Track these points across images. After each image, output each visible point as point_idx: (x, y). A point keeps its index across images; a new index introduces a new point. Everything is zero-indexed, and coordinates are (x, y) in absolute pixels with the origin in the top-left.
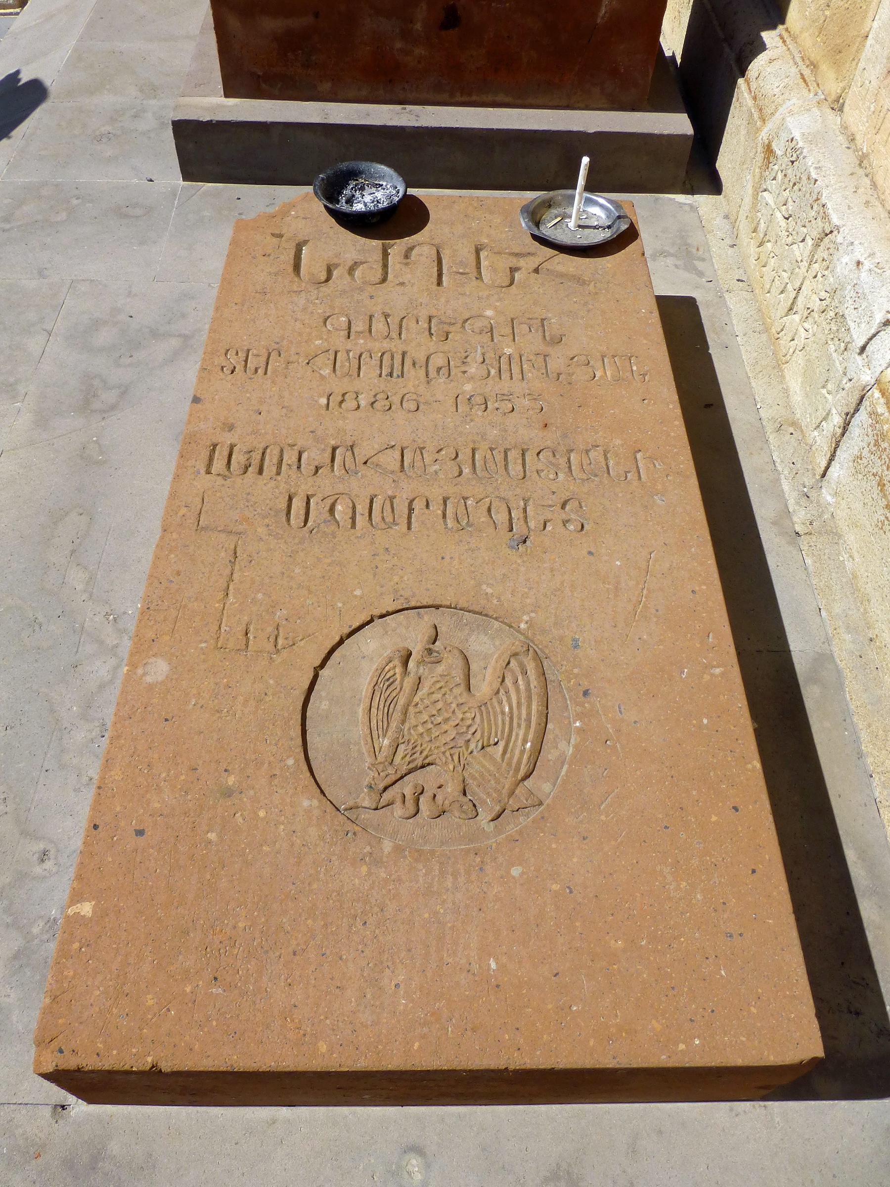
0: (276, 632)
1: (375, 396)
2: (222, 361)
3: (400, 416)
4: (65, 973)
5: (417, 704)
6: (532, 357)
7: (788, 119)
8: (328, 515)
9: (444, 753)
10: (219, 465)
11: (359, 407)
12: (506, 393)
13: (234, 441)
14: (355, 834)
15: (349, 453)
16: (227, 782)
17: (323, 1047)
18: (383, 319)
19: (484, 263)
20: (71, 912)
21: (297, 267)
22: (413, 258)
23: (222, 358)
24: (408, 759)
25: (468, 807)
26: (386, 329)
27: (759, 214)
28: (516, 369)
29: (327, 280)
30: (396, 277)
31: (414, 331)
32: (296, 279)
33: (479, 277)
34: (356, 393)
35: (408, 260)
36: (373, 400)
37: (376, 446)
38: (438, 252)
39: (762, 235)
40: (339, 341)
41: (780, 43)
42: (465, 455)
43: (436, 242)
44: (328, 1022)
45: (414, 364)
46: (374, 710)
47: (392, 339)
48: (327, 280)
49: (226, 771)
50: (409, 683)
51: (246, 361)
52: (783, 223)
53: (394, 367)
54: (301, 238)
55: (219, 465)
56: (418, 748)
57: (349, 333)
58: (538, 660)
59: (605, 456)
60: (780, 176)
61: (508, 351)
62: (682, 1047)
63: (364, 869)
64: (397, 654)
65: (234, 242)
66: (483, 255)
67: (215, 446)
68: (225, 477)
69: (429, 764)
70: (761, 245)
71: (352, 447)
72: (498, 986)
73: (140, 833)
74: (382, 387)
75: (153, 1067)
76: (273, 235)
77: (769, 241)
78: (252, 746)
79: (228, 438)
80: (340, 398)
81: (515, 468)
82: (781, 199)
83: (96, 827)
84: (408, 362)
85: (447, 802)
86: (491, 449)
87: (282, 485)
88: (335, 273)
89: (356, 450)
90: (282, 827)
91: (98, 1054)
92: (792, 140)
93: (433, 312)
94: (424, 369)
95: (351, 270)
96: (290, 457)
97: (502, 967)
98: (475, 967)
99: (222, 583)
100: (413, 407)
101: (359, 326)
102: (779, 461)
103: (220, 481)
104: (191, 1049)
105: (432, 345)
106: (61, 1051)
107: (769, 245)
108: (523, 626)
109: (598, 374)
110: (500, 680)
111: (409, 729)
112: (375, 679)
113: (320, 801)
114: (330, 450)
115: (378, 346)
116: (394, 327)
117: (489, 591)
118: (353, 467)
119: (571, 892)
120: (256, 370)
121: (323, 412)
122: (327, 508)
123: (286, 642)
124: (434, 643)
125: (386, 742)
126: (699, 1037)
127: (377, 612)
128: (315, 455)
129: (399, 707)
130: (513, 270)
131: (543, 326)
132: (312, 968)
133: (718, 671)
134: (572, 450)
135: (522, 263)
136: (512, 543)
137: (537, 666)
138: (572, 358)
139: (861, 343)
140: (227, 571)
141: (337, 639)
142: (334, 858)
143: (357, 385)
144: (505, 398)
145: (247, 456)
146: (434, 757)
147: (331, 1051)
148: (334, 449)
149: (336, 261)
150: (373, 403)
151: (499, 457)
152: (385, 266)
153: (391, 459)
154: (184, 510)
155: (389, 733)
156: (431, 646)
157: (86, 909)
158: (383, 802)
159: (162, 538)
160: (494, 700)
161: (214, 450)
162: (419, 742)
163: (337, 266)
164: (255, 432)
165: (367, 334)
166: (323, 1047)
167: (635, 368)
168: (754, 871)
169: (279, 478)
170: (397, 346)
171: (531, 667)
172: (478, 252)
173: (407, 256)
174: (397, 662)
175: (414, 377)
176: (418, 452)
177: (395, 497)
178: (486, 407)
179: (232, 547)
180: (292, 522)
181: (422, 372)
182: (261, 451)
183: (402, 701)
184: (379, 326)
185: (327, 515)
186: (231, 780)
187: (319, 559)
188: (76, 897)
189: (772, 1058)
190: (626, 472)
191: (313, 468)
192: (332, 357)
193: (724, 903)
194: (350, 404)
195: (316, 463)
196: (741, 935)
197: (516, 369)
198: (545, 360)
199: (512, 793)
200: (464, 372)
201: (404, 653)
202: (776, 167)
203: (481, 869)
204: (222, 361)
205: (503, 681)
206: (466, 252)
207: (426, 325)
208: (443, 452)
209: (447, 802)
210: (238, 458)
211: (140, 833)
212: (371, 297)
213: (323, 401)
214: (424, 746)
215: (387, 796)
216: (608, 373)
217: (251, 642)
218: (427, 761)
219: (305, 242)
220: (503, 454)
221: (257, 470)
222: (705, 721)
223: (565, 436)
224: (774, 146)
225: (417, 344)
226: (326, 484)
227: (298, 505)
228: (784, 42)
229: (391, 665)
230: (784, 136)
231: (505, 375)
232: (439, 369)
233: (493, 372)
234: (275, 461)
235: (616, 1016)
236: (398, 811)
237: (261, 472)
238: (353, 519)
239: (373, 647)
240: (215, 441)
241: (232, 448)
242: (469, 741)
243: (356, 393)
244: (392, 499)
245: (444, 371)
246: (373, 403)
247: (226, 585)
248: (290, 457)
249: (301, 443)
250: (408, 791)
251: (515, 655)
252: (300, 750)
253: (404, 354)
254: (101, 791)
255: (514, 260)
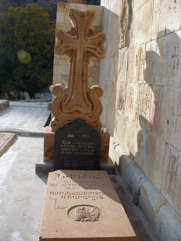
139: (138, 182)
194: (69, 188)
237: (58, 194)
239: (76, 209)
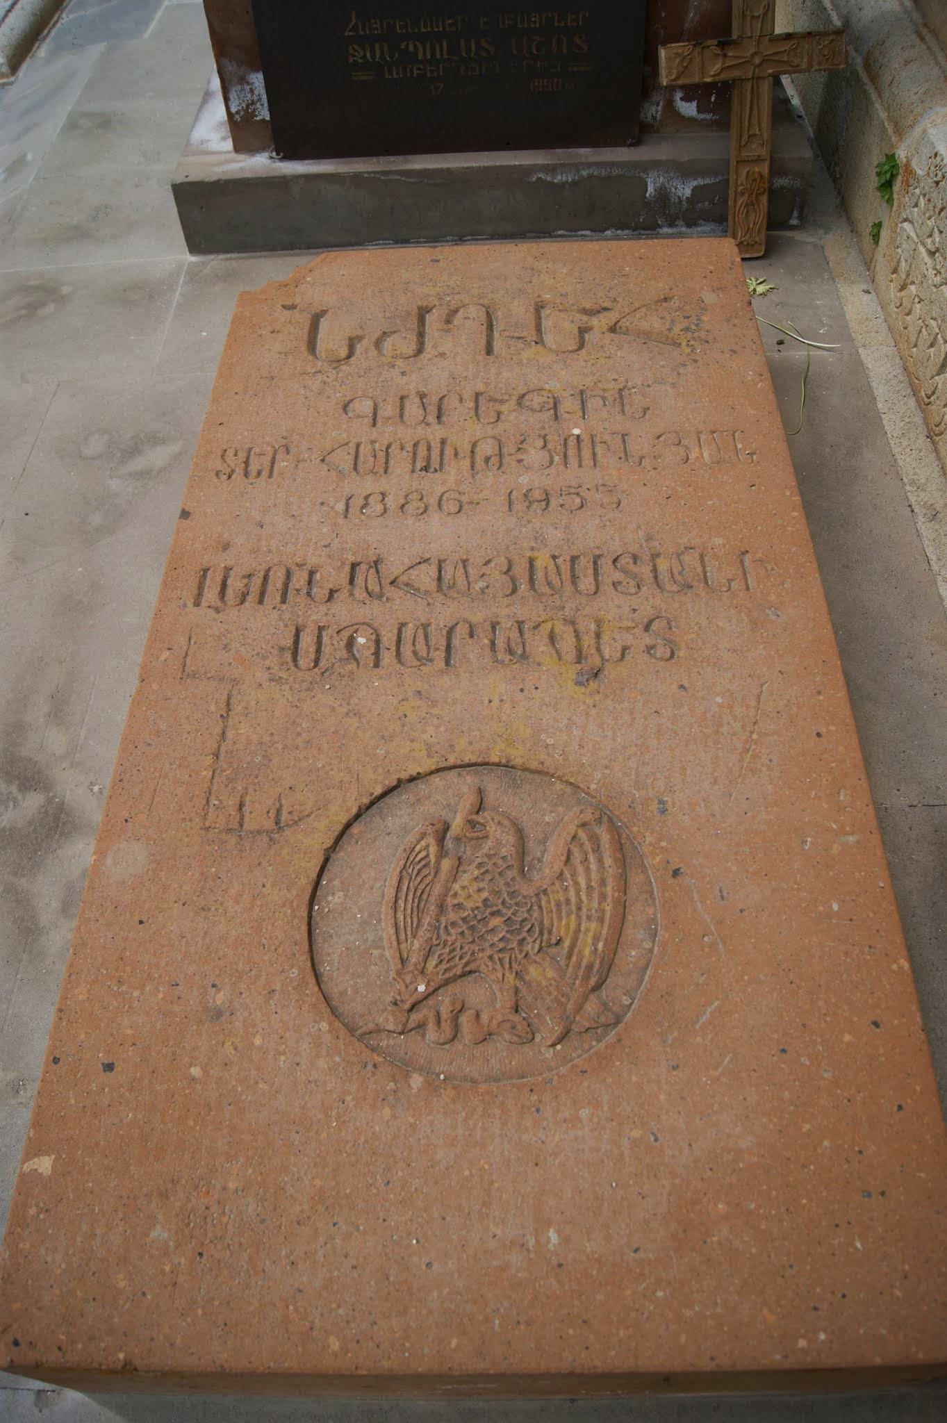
0: (277, 805)
1: (407, 496)
2: (218, 464)
3: (435, 518)
4: (21, 1246)
5: (455, 895)
6: (607, 438)
7: (930, 131)
8: (344, 651)
9: (491, 957)
10: (211, 595)
11: (385, 511)
12: (573, 484)
13: (229, 563)
14: (375, 1066)
15: (373, 571)
16: (214, 1001)
17: (335, 1344)
18: (417, 400)
19: (547, 324)
20: (27, 1167)
21: (312, 345)
22: (456, 323)
23: (218, 461)
24: (444, 966)
25: (521, 1028)
26: (421, 411)
27: (899, 250)
28: (586, 453)
29: (349, 357)
30: (434, 347)
31: (458, 411)
32: (311, 358)
33: (539, 341)
34: (382, 494)
35: (450, 326)
36: (403, 501)
37: (406, 561)
38: (488, 313)
39: (904, 277)
40: (361, 431)
41: (917, 41)
42: (520, 570)
43: (486, 302)
44: (341, 1311)
45: (456, 454)
46: (401, 903)
47: (428, 424)
48: (349, 357)
49: (214, 986)
50: (446, 864)
51: (247, 463)
52: (928, 260)
53: (428, 462)
54: (316, 309)
55: (211, 595)
56: (458, 952)
57: (374, 419)
58: (615, 830)
59: (702, 561)
60: (922, 202)
61: (576, 431)
62: (802, 1343)
63: (387, 1112)
64: (430, 830)
65: (237, 321)
66: (544, 313)
67: (206, 571)
68: (217, 610)
69: (470, 972)
70: (903, 288)
71: (376, 563)
72: (560, 1265)
73: (109, 1067)
74: (415, 485)
75: (125, 1365)
76: (284, 307)
77: (913, 283)
78: (246, 953)
79: (221, 561)
80: (362, 502)
81: (586, 583)
82: (926, 230)
83: (56, 1061)
84: (449, 451)
85: (495, 1022)
86: (554, 557)
87: (287, 616)
88: (359, 348)
89: (382, 567)
90: (283, 1058)
91: (60, 1349)
92: (936, 155)
93: (480, 387)
94: (468, 461)
95: (378, 343)
96: (299, 580)
97: (565, 1240)
98: (531, 1241)
99: (211, 744)
100: (454, 509)
101: (388, 410)
102: (934, 558)
103: (211, 612)
104: (172, 1345)
105: (476, 430)
106: (16, 1343)
107: (913, 288)
108: (593, 787)
109: (692, 456)
110: (564, 858)
111: (446, 927)
112: (403, 862)
113: (330, 1024)
114: (347, 568)
115: (408, 434)
116: (432, 409)
117: (550, 741)
118: (377, 589)
119: (656, 1140)
120: (259, 473)
121: (341, 520)
122: (343, 643)
123: (290, 817)
124: (477, 813)
125: (417, 944)
126: (825, 1331)
127: (404, 776)
128: (332, 575)
129: (432, 899)
130: (583, 331)
131: (621, 397)
132: (322, 1240)
133: (851, 839)
134: (658, 555)
135: (594, 321)
136: (580, 679)
137: (613, 838)
138: (659, 437)
140: (218, 730)
141: (354, 811)
142: (348, 1098)
143: (383, 484)
144: (573, 490)
145: (245, 581)
146: (478, 963)
147: (344, 1350)
148: (354, 566)
149: (360, 332)
150: (402, 506)
151: (566, 568)
152: (421, 335)
153: (425, 577)
154: (165, 654)
155: (421, 933)
156: (474, 817)
157: (44, 1164)
158: (411, 1024)
159: (139, 692)
160: (749, 85)
161: (204, 576)
162: (458, 945)
163: (360, 338)
164: (255, 551)
165: (397, 419)
166: (335, 1344)
167: (740, 446)
168: (900, 1108)
169: (284, 607)
170: (435, 433)
171: (605, 838)
172: (539, 307)
173: (448, 321)
174: (431, 840)
175: (455, 471)
176: (460, 565)
177: (429, 625)
178: (547, 504)
179: (225, 697)
180: (301, 662)
181: (467, 462)
182: (262, 573)
183: (437, 889)
184: (413, 408)
185: (343, 653)
186: (221, 998)
187: (333, 709)
188: (34, 1150)
189: (921, 1356)
190: (730, 581)
191: (327, 592)
192: (353, 451)
193: (860, 1152)
195: (331, 586)
196: (883, 1194)
197: (586, 453)
198: (624, 441)
199: (579, 1008)
200: (520, 461)
201: (439, 826)
202: (917, 191)
203: (538, 1110)
204: (218, 464)
205: (568, 859)
206: (521, 310)
207: (472, 405)
208: (493, 564)
209: (495, 1022)
210: (235, 584)
211: (109, 1067)
212: (403, 374)
213: (340, 507)
214: (466, 949)
215: (415, 1018)
216: (706, 455)
217: (247, 819)
218: (468, 969)
219: (324, 313)
220: (568, 564)
221: (257, 599)
222: (835, 907)
223: (649, 538)
224: (914, 164)
225: (463, 429)
226: (342, 611)
227: (307, 640)
228: (922, 39)
229: (423, 843)
230: (926, 151)
231: (573, 460)
232: (487, 459)
233: (556, 459)
234: (279, 585)
235: (716, 1303)
236: (431, 1034)
238: (377, 654)
239: (403, 823)
240: (206, 565)
241: (228, 569)
242: (524, 939)
243: (382, 494)
244: (425, 626)
245: (494, 460)
246: (402, 506)
247: (216, 746)
248: (299, 580)
249: (312, 561)
250: (445, 1011)
251: (584, 825)
252: (304, 958)
253: (443, 442)
254: (62, 1015)
255: (585, 318)
